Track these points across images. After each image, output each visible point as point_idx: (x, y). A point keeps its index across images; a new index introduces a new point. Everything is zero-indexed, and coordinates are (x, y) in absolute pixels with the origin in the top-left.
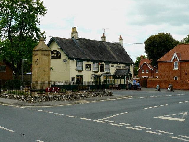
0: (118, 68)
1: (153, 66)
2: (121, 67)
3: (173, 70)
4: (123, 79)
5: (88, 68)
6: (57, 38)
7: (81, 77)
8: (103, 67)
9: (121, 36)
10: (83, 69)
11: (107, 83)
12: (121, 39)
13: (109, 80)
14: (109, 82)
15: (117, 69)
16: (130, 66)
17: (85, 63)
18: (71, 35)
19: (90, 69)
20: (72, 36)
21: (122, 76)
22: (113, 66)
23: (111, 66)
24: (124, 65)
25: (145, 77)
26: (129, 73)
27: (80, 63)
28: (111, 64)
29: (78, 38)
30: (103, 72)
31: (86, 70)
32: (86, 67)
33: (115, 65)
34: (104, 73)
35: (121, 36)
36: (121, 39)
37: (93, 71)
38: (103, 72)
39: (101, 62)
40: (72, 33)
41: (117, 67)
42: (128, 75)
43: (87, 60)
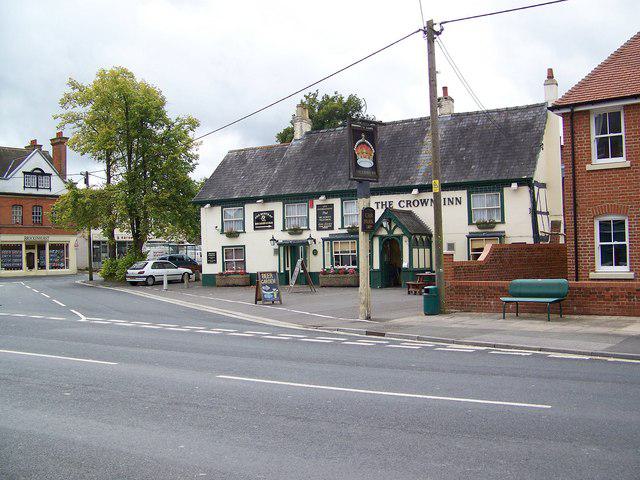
3: (589, 167)
4: (427, 250)
5: (264, 221)
7: (240, 250)
8: (331, 213)
9: (550, 71)
10: (310, 223)
16: (506, 190)
17: (250, 209)
19: (273, 225)
27: (231, 212)
30: (332, 228)
31: (255, 229)
32: (258, 220)
34: (337, 230)
35: (550, 71)
37: (284, 230)
38: (332, 228)
39: (317, 196)
43: (253, 200)
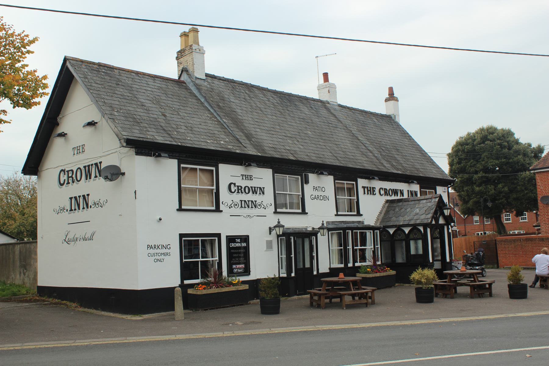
0: (393, 198)
1: (291, 238)
2: (402, 194)
6: (136, 71)
11: (350, 265)
12: (391, 97)
13: (354, 251)
14: (355, 261)
15: (387, 201)
18: (179, 64)
20: (181, 68)
21: (414, 227)
22: (371, 191)
23: (361, 191)
24: (416, 187)
25: (480, 233)
26: (443, 214)
28: (362, 183)
29: (207, 75)
33: (378, 184)
36: (391, 97)
40: (181, 54)
41: (386, 192)
42: (437, 220)
